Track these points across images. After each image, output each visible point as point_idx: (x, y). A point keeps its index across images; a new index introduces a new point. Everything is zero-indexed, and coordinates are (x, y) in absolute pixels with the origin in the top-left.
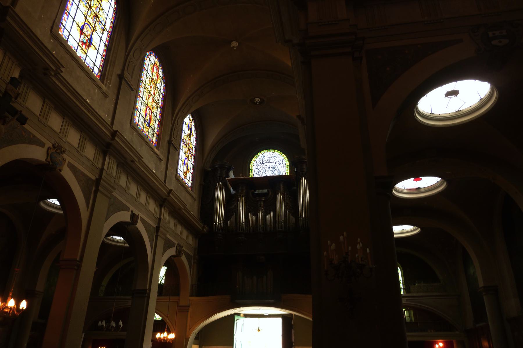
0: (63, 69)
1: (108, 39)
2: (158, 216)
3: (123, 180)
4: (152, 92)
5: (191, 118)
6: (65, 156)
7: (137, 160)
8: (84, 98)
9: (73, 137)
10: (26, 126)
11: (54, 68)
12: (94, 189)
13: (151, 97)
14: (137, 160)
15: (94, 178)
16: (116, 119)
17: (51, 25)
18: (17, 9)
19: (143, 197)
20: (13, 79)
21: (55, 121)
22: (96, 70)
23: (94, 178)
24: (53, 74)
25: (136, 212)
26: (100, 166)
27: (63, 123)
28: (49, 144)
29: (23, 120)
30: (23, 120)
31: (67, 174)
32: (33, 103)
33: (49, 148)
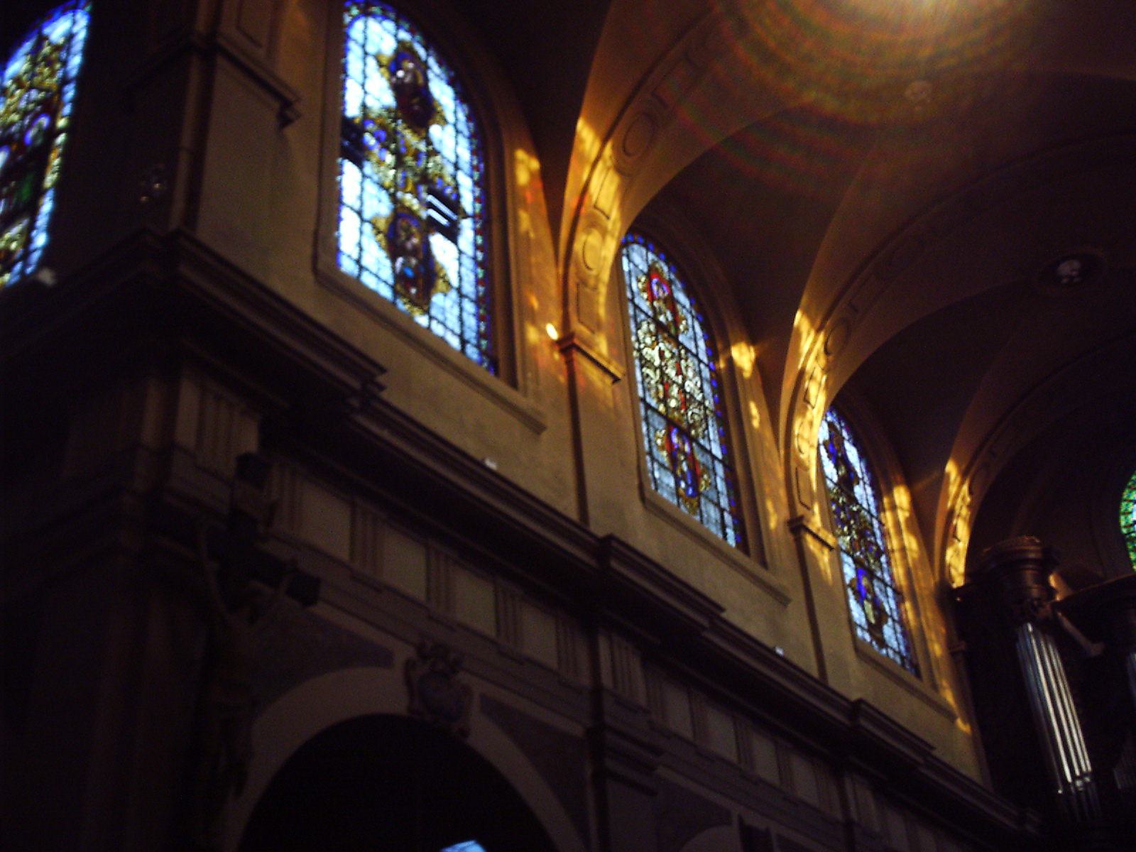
0: (381, 379)
1: (480, 240)
2: (839, 815)
3: (678, 711)
4: (671, 372)
5: (82, 35)
6: (463, 678)
7: (705, 623)
8: (478, 457)
9: (475, 600)
10: (321, 609)
11: (356, 384)
12: (588, 771)
13: (675, 391)
14: (705, 623)
15: (577, 730)
16: (817, 608)
17: (308, 251)
18: (204, 233)
19: (764, 755)
20: (244, 460)
21: (405, 563)
22: (472, 352)
23: (577, 730)
24: (355, 402)
25: (756, 821)
26: (585, 681)
27: (353, 521)
28: (403, 653)
29: (307, 590)
30: (307, 590)
31: (487, 739)
32: (323, 521)
33: (409, 666)
